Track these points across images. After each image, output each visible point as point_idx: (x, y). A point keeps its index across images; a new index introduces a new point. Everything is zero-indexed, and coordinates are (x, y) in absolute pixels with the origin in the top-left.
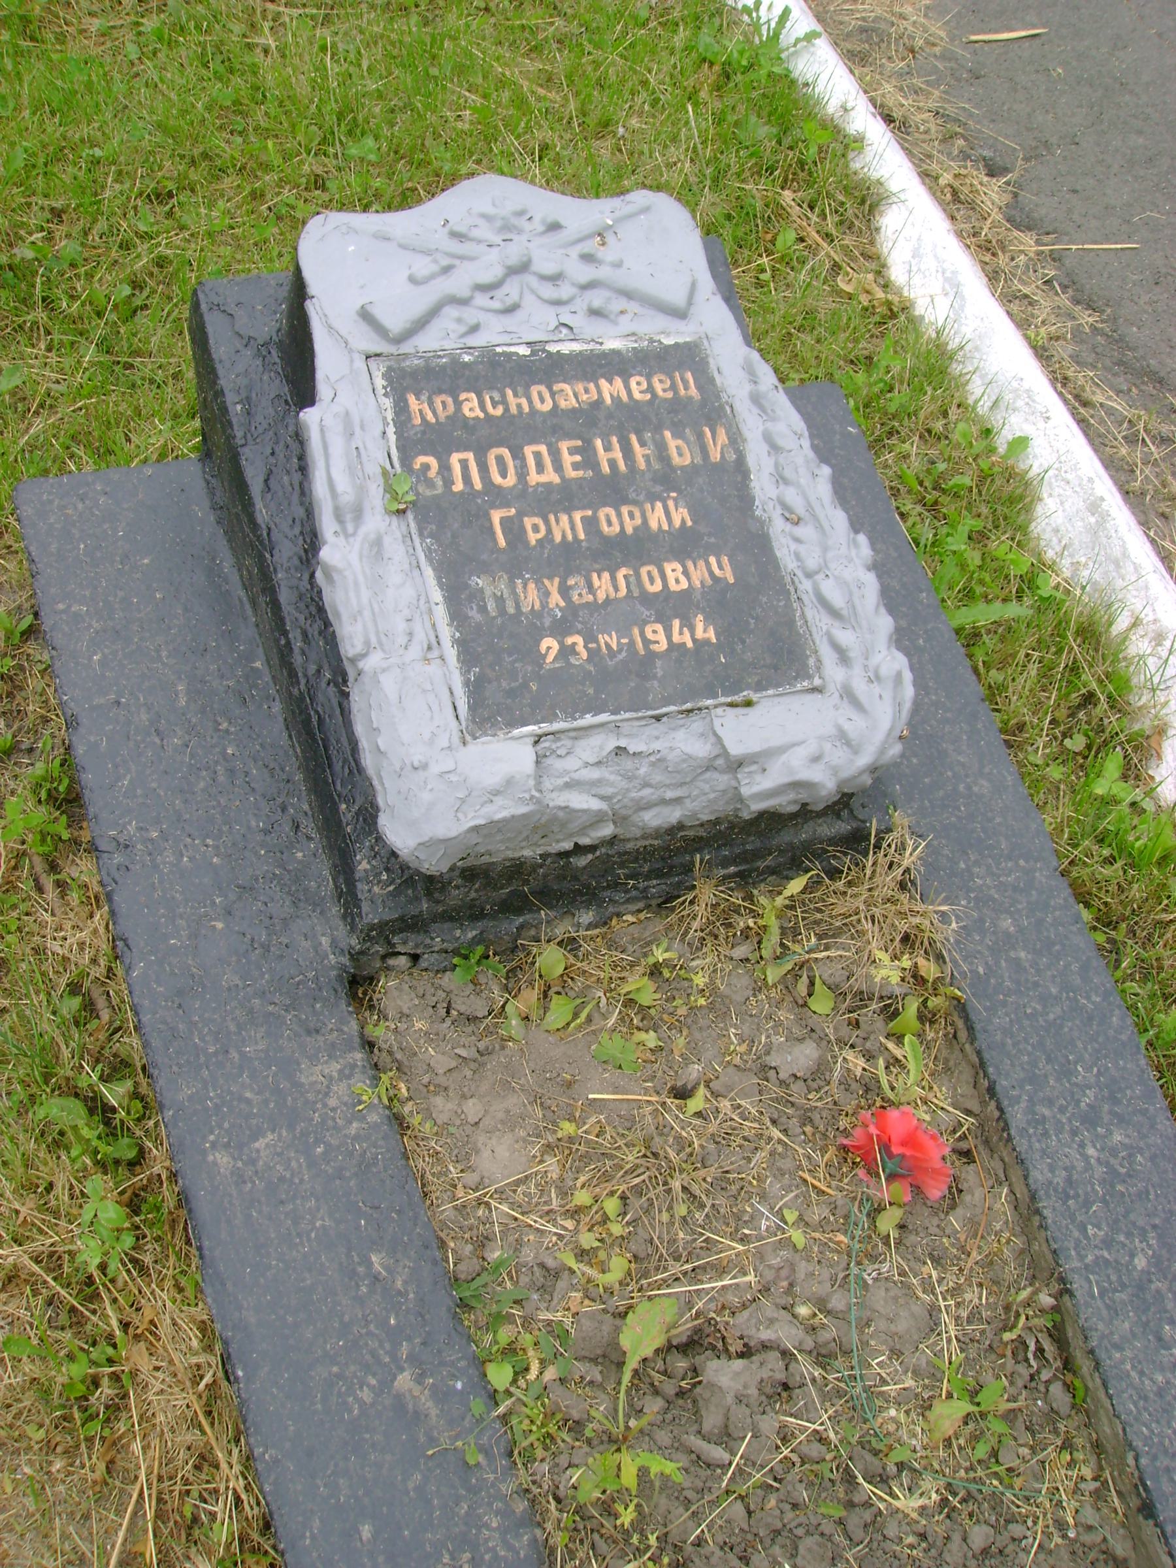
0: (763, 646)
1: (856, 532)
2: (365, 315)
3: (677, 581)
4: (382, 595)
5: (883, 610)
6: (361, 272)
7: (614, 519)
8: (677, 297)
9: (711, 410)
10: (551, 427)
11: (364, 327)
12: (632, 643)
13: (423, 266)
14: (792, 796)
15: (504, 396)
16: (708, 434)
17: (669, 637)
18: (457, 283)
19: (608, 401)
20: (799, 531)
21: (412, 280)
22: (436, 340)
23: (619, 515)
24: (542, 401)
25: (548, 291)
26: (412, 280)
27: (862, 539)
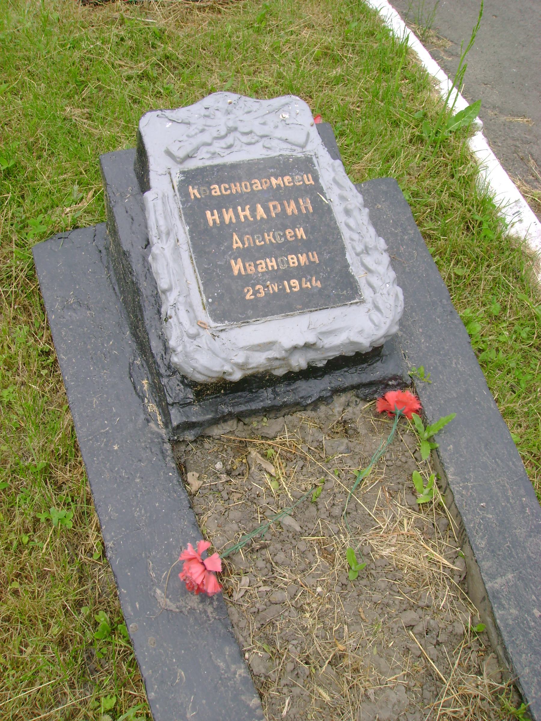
0: (341, 288)
1: (365, 206)
2: (168, 153)
3: (293, 263)
4: (173, 266)
5: (390, 268)
6: (160, 131)
9: (315, 191)
10: (250, 199)
11: (168, 158)
12: (284, 289)
14: (352, 348)
17: (300, 285)
18: (206, 137)
23: (220, 188)
24: (246, 188)
25: (245, 139)
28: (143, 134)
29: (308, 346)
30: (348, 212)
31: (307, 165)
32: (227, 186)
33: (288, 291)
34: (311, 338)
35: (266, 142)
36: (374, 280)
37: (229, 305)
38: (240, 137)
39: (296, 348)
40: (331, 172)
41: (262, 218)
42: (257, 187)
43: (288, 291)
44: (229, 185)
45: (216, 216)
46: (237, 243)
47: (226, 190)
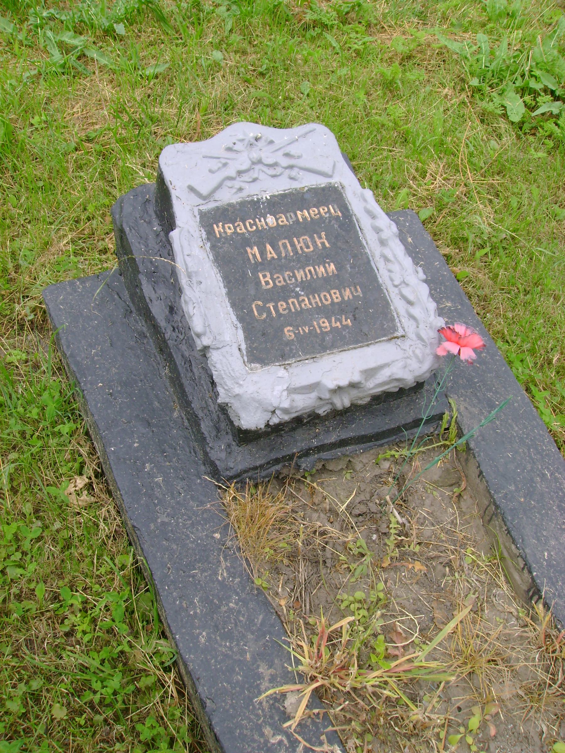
0: (370, 319)
3: (337, 298)
4: (210, 312)
6: (194, 171)
7: (328, 296)
8: (327, 168)
13: (214, 165)
14: (396, 384)
15: (254, 220)
16: (327, 245)
17: (331, 326)
18: (231, 171)
19: (301, 220)
20: (390, 266)
21: (211, 171)
22: (227, 197)
25: (271, 172)
26: (211, 171)
27: (420, 270)
28: (168, 177)
29: (353, 386)
30: (383, 243)
31: (331, 194)
32: (252, 222)
33: (318, 331)
34: (356, 378)
35: (294, 173)
36: (416, 311)
37: (265, 346)
38: (265, 169)
39: (339, 389)
40: (361, 201)
41: (273, 258)
42: (282, 221)
43: (318, 331)
44: (254, 220)
45: (318, 242)
46: (271, 253)
47: (251, 227)
